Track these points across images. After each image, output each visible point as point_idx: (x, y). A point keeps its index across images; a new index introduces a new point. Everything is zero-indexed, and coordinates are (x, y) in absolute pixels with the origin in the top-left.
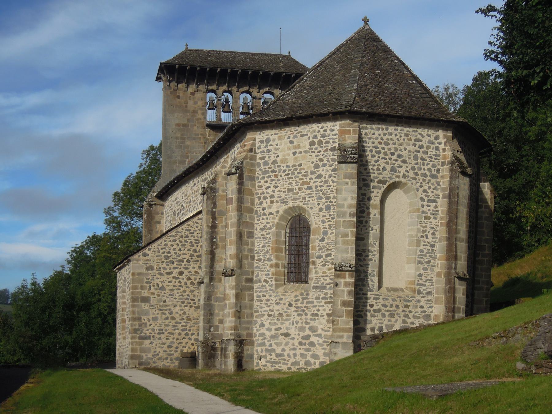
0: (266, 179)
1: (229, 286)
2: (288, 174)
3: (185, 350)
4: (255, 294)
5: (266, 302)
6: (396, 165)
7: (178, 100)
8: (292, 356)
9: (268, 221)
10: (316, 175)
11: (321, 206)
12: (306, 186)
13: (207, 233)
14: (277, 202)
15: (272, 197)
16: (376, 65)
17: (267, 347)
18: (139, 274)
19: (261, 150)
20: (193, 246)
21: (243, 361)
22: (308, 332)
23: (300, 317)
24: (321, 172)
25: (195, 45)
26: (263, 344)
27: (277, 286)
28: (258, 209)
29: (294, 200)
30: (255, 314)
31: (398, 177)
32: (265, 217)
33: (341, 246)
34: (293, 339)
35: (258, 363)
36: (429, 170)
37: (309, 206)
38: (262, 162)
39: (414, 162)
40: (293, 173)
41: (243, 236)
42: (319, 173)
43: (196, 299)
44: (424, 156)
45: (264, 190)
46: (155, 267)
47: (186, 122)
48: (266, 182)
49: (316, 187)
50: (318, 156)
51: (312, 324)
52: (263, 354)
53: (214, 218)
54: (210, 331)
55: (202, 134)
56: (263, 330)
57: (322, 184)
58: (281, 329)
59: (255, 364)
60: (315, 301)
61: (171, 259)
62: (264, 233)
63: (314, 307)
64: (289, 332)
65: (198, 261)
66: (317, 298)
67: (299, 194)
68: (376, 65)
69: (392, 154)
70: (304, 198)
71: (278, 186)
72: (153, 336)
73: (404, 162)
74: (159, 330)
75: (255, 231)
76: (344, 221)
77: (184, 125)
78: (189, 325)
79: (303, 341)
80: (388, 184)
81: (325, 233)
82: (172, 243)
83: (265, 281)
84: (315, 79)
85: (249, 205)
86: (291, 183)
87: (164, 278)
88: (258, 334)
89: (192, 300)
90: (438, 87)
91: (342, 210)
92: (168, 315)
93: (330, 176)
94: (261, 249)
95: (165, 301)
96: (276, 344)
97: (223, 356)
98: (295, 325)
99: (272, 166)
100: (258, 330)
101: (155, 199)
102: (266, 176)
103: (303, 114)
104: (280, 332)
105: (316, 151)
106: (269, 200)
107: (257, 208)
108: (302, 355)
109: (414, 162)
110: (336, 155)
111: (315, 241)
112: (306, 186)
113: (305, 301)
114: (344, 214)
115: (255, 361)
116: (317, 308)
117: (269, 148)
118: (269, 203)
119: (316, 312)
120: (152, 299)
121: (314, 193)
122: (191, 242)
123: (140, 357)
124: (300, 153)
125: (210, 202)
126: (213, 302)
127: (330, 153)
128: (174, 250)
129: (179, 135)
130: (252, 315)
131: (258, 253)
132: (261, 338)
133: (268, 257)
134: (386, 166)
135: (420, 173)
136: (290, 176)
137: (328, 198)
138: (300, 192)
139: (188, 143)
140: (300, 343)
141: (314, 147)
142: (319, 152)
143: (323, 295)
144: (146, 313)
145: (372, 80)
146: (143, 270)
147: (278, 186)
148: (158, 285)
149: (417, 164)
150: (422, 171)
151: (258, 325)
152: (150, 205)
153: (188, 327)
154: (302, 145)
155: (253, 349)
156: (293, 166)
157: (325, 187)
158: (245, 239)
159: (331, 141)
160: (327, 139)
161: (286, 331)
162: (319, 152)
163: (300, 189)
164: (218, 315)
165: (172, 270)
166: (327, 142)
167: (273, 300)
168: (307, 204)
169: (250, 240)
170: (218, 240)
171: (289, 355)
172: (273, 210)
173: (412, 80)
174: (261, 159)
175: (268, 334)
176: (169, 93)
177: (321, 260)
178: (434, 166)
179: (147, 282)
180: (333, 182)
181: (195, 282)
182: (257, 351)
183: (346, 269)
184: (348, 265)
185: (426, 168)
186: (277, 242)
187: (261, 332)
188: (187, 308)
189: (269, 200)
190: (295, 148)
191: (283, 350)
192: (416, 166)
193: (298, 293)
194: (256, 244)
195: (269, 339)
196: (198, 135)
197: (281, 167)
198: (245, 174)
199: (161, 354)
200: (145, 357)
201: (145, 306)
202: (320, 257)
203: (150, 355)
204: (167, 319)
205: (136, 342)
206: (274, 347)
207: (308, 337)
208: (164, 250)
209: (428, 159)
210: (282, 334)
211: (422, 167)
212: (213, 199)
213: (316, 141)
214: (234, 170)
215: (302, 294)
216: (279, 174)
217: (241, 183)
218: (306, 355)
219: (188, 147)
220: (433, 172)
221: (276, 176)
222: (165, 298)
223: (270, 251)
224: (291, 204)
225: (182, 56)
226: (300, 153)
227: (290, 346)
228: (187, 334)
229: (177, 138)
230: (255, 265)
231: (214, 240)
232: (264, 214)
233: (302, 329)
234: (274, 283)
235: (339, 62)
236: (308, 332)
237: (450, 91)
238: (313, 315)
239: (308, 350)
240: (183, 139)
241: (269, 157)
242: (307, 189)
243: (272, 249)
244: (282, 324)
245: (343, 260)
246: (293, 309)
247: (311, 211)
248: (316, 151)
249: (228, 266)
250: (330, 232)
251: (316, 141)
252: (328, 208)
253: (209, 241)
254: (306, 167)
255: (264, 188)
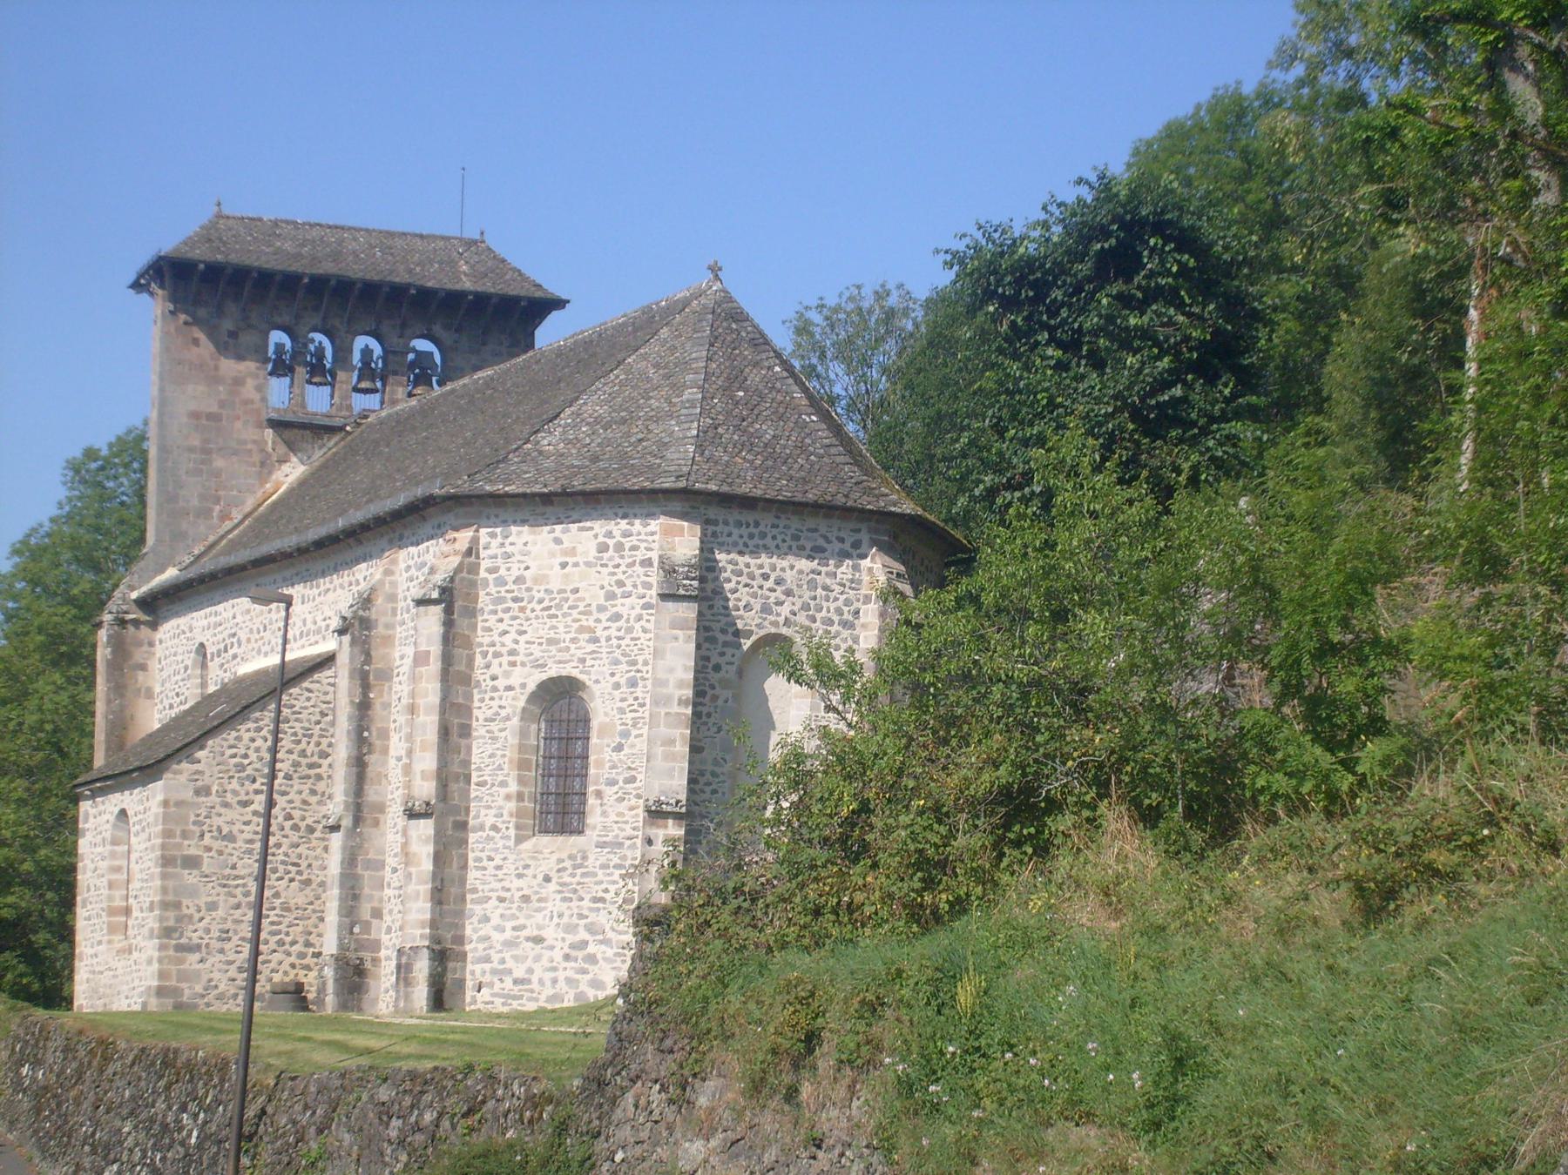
0: (500, 615)
1: (419, 837)
2: (549, 608)
3: (277, 978)
4: (471, 856)
5: (494, 872)
6: (772, 600)
7: (195, 350)
8: (548, 983)
9: (503, 703)
10: (608, 614)
11: (616, 679)
12: (586, 636)
13: (350, 718)
14: (523, 664)
15: (512, 653)
16: (736, 379)
17: (495, 965)
18: (179, 804)
19: (489, 552)
20: (299, 742)
21: (446, 994)
22: (583, 935)
23: (566, 905)
24: (619, 609)
25: (240, 206)
26: (488, 960)
27: (520, 840)
28: (481, 678)
29: (560, 662)
30: (469, 897)
31: (775, 624)
32: (495, 695)
33: (659, 763)
34: (552, 948)
35: (474, 997)
36: (839, 611)
37: (594, 678)
38: (491, 577)
39: (807, 595)
40: (559, 607)
41: (453, 730)
42: (615, 610)
43: (304, 864)
44: (828, 581)
45: (496, 638)
46: (214, 788)
47: (214, 409)
48: (501, 620)
49: (609, 639)
50: (614, 574)
51: (592, 917)
52: (487, 978)
53: (366, 686)
54: (352, 933)
55: (255, 442)
56: (486, 933)
57: (621, 634)
58: (524, 927)
59: (468, 999)
60: (600, 872)
61: (249, 771)
62: (494, 726)
63: (596, 883)
64: (544, 933)
65: (309, 777)
66: (603, 867)
67: (573, 651)
68: (736, 379)
69: (766, 577)
70: (583, 661)
71: (525, 632)
72: (207, 945)
73: (788, 593)
74: (222, 931)
75: (474, 724)
76: (667, 714)
77: (212, 417)
78: (286, 921)
79: (574, 953)
80: (754, 638)
81: (625, 734)
82: (252, 734)
83: (495, 828)
84: (607, 402)
85: (463, 668)
86: (553, 627)
87: (230, 814)
88: (475, 937)
89: (294, 864)
90: (859, 287)
91: (665, 691)
92: (240, 897)
93: (639, 618)
94: (487, 761)
95: (234, 867)
96: (516, 958)
97: (402, 983)
98: (556, 920)
99: (514, 587)
100: (475, 930)
101: (134, 607)
102: (500, 607)
103: (589, 487)
104: (525, 933)
105: (611, 564)
106: (505, 659)
107: (478, 674)
108: (569, 981)
109: (807, 595)
110: (655, 577)
111: (601, 751)
112: (586, 636)
113: (579, 871)
114: (667, 700)
115: (469, 994)
116: (604, 886)
117: (509, 549)
118: (505, 667)
119: (600, 894)
120: (206, 861)
121: (604, 650)
122: (295, 734)
123: (176, 992)
124: (576, 565)
125: (357, 650)
126: (359, 870)
127: (639, 569)
128: (257, 750)
129: (196, 443)
130: (463, 899)
131: (479, 769)
132: (481, 946)
133: (500, 778)
134: (752, 601)
135: (819, 616)
136: (553, 611)
137: (633, 663)
138: (573, 646)
139: (219, 463)
140: (567, 957)
141: (605, 555)
142: (618, 566)
143: (616, 860)
144: (194, 893)
145: (729, 413)
146: (188, 795)
147: (525, 632)
148: (220, 830)
149: (815, 598)
150: (824, 613)
151: (475, 919)
152: (122, 622)
153: (282, 927)
154: (580, 549)
155: (464, 968)
156: (561, 591)
157: (627, 641)
158: (454, 738)
159: (643, 545)
160: (634, 540)
161: (536, 933)
162: (618, 566)
163: (573, 640)
164: (371, 897)
165: (252, 796)
166: (634, 548)
167: (509, 868)
168: (588, 673)
169: (463, 742)
170: (372, 735)
171: (541, 982)
172: (515, 681)
173: (809, 415)
174: (491, 571)
175: (497, 937)
176: (172, 330)
177: (615, 788)
178: (847, 603)
179: (195, 823)
180: (645, 631)
181: (303, 825)
182: (473, 973)
183: (669, 809)
184: (673, 801)
185: (833, 606)
186: (522, 748)
187: (481, 933)
188: (284, 883)
189: (505, 659)
190: (565, 553)
191: (530, 971)
192: (812, 603)
193: (564, 855)
194: (475, 750)
195: (499, 947)
196: (245, 442)
197: (534, 592)
198: (458, 605)
199: (222, 987)
200: (187, 992)
201: (190, 878)
202: (612, 783)
203: (199, 989)
204: (238, 906)
205: (168, 957)
206: (510, 964)
207: (584, 944)
208: (234, 751)
209: (838, 589)
210: (528, 939)
211: (825, 604)
212: (365, 642)
213: (611, 542)
214: (435, 595)
215: (571, 857)
216: (530, 606)
217: (448, 623)
218: (578, 981)
219: (217, 474)
220: (846, 616)
221: (522, 609)
222: (235, 859)
223: (506, 767)
224: (553, 671)
225: (208, 234)
226: (576, 565)
227: (545, 962)
228: (281, 943)
229: (191, 450)
230: (473, 795)
231: (366, 734)
232: (495, 689)
233: (571, 929)
234: (512, 832)
235: (657, 366)
236: (583, 935)
237: (893, 300)
238: (596, 900)
239: (584, 972)
240: (208, 452)
241: (509, 569)
242: (589, 641)
243: (511, 762)
244: (529, 917)
245: (663, 793)
246: (552, 886)
247: (596, 688)
248: (611, 564)
249: (416, 792)
250: (634, 732)
251: (611, 542)
252: (633, 683)
253: (353, 736)
254: (587, 595)
255: (495, 633)
